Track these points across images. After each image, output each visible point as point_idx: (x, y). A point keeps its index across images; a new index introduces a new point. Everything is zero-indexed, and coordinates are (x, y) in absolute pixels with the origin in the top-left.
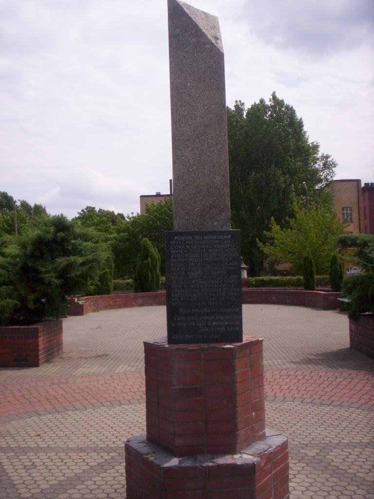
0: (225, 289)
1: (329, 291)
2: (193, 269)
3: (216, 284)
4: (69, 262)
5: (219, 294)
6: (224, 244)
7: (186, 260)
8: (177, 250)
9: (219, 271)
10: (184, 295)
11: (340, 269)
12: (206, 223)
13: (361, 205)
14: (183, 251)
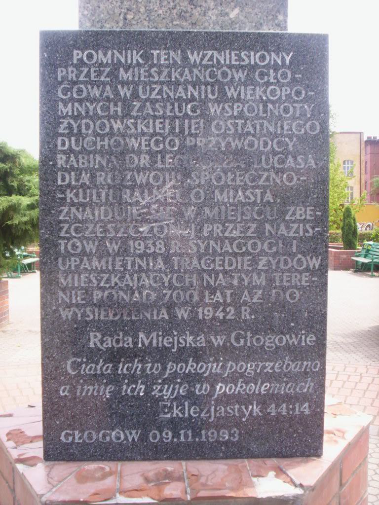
0: (263, 261)
1: (340, 248)
2: (141, 179)
3: (232, 240)
4: (10, 203)
5: (241, 280)
6: (268, 84)
7: (118, 144)
8: (80, 101)
9: (244, 191)
10: (108, 281)
11: (355, 223)
12: (196, 12)
13: (363, 158)
14: (106, 109)
